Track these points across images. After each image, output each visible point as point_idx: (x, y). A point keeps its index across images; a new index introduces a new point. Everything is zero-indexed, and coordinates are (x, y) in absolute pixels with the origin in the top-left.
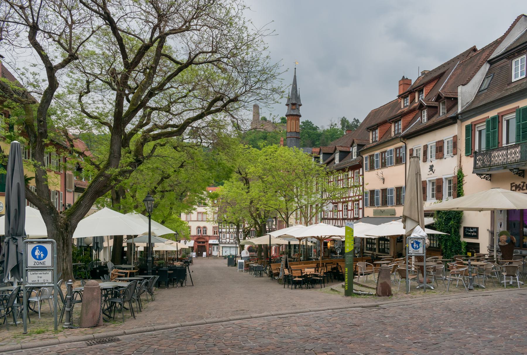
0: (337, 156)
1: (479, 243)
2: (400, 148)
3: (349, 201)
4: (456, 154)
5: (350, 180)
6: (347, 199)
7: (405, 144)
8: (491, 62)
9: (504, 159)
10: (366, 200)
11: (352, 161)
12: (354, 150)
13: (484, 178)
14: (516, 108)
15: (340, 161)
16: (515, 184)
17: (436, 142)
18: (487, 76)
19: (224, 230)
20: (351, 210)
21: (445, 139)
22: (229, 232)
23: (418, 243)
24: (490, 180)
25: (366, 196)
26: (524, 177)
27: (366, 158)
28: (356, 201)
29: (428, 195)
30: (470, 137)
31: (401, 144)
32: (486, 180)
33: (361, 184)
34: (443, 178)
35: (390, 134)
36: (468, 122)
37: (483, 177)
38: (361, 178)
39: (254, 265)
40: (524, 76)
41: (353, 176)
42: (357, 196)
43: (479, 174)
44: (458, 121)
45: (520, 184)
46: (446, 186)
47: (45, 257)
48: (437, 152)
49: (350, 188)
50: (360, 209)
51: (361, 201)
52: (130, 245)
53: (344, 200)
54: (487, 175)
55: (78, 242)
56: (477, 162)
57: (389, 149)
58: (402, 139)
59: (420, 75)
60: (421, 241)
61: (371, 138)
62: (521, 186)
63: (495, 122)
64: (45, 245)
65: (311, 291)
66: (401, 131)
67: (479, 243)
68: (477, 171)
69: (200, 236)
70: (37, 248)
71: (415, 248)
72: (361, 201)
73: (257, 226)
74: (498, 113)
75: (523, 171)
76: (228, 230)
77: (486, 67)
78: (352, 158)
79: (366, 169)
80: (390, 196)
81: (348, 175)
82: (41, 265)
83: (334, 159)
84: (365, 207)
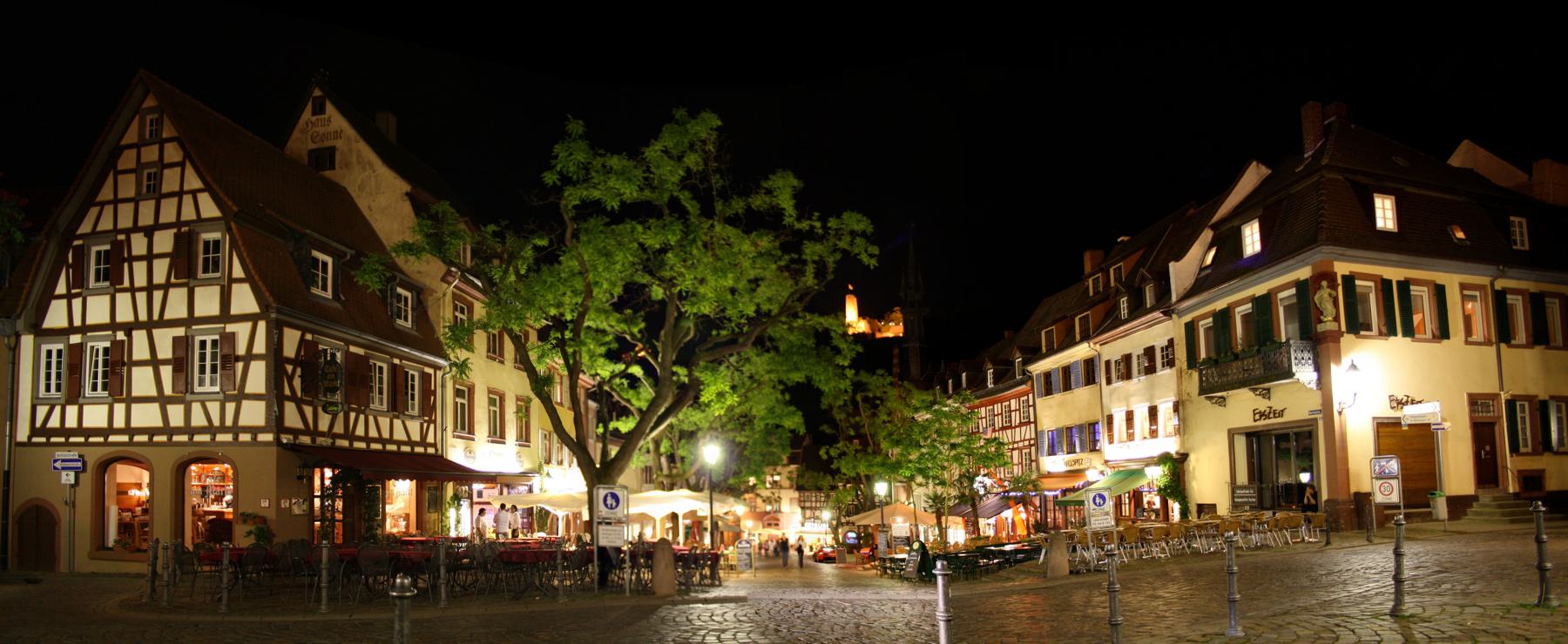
1: (1215, 505)
8: (1213, 227)
13: (1259, 395)
23: (1102, 497)
33: (1032, 420)
34: (1400, 335)
37: (1214, 401)
38: (1031, 409)
39: (1401, 164)
49: (1016, 427)
50: (1032, 461)
55: (686, 519)
60: (1106, 494)
65: (1068, 361)
67: (1215, 505)
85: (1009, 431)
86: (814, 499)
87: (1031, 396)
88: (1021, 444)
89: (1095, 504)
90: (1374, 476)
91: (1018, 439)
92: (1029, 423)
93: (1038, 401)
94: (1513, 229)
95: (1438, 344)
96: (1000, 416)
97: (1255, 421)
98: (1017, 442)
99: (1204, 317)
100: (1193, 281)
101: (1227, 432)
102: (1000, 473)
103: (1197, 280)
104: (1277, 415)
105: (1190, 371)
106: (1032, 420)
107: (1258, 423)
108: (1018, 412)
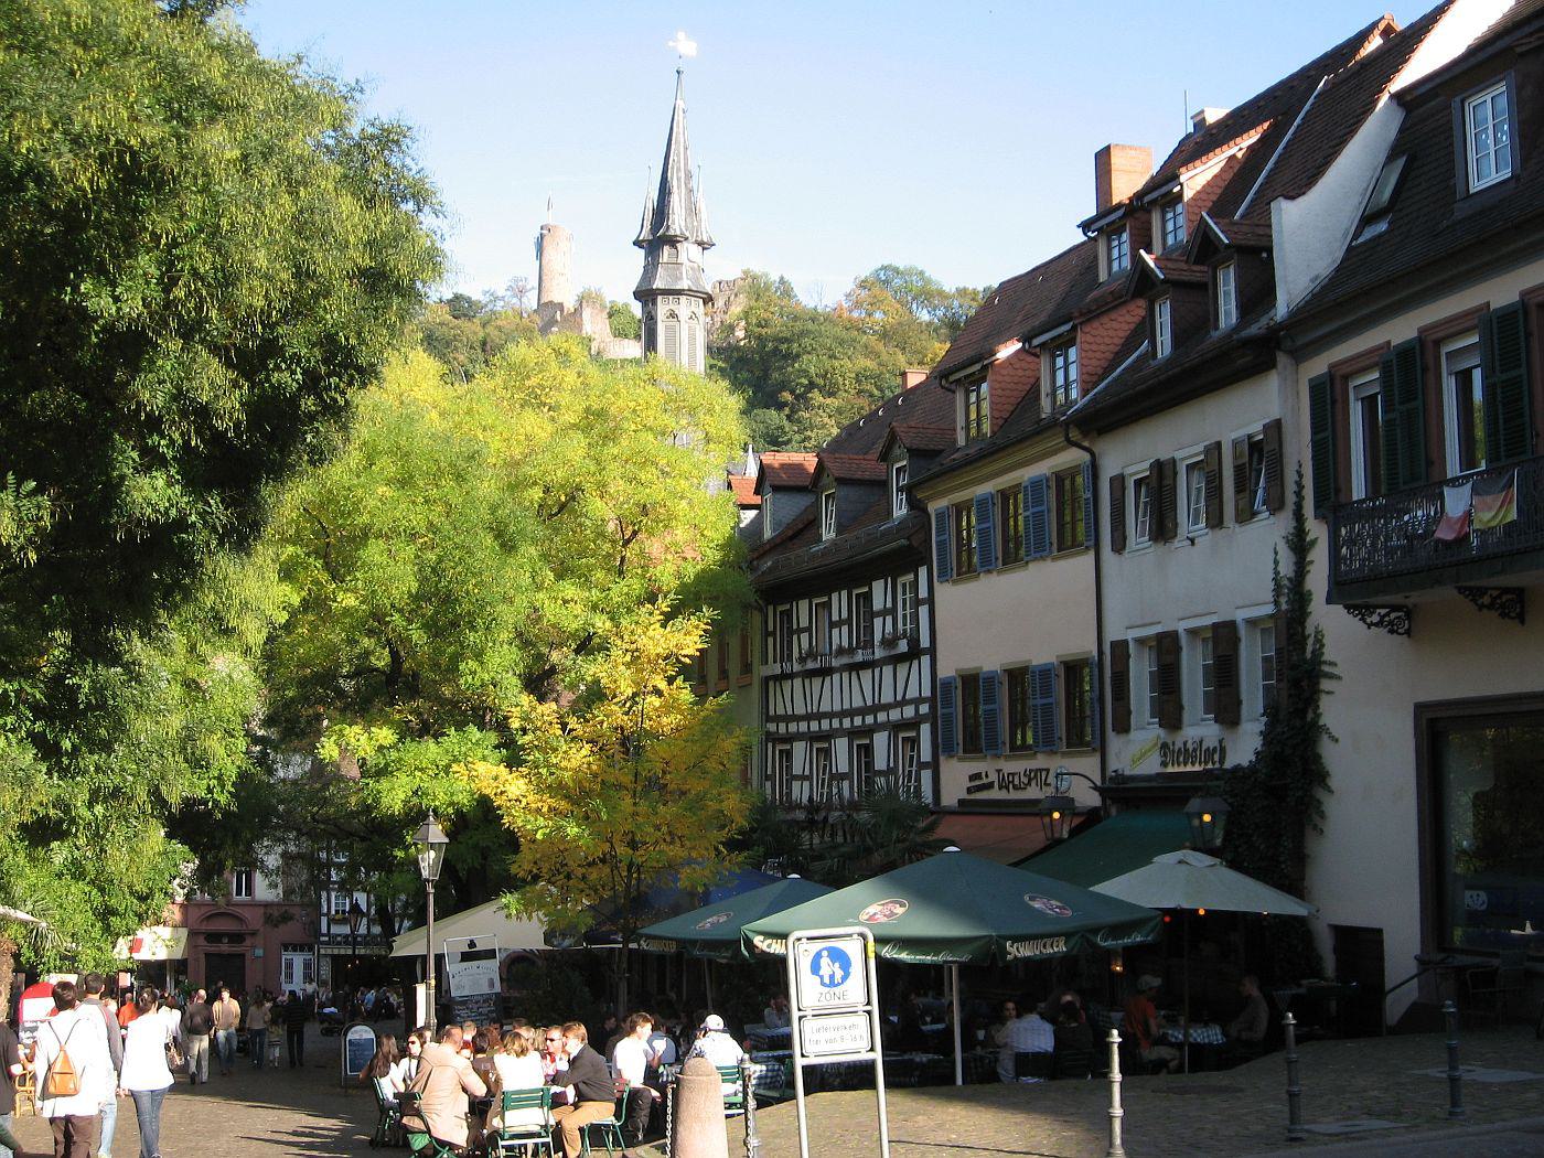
1: (1380, 931)
2: (1072, 472)
3: (877, 727)
6: (869, 720)
7: (1093, 454)
10: (948, 719)
11: (814, 556)
13: (1490, 607)
14: (1478, 309)
21: (1183, 459)
24: (1408, 632)
25: (948, 702)
26: (1522, 622)
27: (940, 515)
29: (1185, 701)
30: (1523, 370)
31: (1071, 457)
32: (1391, 632)
34: (1181, 630)
35: (1039, 409)
36: (1318, 366)
37: (1486, 600)
38: (923, 611)
40: (1506, 173)
41: (889, 605)
43: (1355, 607)
44: (1282, 359)
51: (925, 729)
52: (740, 833)
53: (858, 721)
54: (1394, 608)
57: (1027, 474)
58: (1074, 434)
59: (1191, 129)
61: (960, 422)
66: (1074, 394)
67: (1380, 931)
70: (825, 953)
71: (827, 980)
72: (925, 729)
74: (1422, 331)
75: (1520, 592)
78: (890, 513)
80: (1040, 702)
81: (868, 597)
82: (837, 1002)
87: (923, 571)
88: (895, 715)
91: (887, 698)
93: (944, 592)
94: (1232, 143)
95: (975, 583)
96: (845, 629)
98: (887, 707)
99: (1358, 364)
100: (1340, 255)
101: (1411, 709)
103: (1350, 249)
106: (925, 642)
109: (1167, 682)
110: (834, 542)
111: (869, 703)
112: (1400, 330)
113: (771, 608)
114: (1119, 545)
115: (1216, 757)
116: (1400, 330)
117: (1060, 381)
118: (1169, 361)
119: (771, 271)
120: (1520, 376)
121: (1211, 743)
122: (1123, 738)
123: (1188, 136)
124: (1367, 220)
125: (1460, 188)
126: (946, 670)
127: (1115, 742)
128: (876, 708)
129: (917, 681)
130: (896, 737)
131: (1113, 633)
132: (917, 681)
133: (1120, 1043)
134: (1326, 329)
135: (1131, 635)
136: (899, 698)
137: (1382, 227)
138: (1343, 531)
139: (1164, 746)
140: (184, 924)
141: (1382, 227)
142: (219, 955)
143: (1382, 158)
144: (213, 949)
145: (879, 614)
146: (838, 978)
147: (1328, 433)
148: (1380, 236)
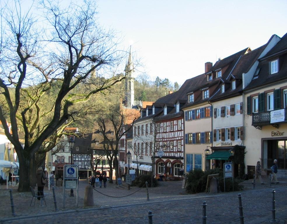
0: (166, 110)
3: (174, 140)
4: (242, 113)
5: (175, 126)
6: (173, 139)
7: (211, 104)
9: (268, 118)
12: (178, 107)
13: (257, 128)
15: (168, 113)
16: (273, 132)
17: (231, 106)
18: (258, 68)
19: (77, 159)
20: (176, 146)
22: (88, 160)
24: (261, 129)
27: (186, 112)
28: (179, 140)
30: (280, 97)
31: (209, 105)
33: (183, 129)
36: (248, 95)
41: (177, 124)
42: (180, 137)
44: (243, 94)
45: (276, 132)
46: (218, 134)
47: (73, 173)
48: (221, 113)
49: (168, 132)
51: (182, 141)
53: (171, 139)
56: (254, 119)
58: (210, 102)
62: (276, 133)
63: (250, 99)
64: (229, 165)
68: (255, 124)
69: (59, 163)
71: (70, 173)
72: (182, 141)
73: (114, 157)
76: (80, 159)
77: (256, 64)
79: (186, 120)
83: (163, 112)
84: (185, 145)
85: (172, 133)
86: (80, 157)
88: (177, 139)
89: (69, 173)
90: (183, 132)
92: (181, 130)
96: (169, 127)
97: (272, 136)
99: (255, 95)
100: (251, 81)
102: (168, 149)
103: (252, 80)
104: (280, 134)
105: (248, 115)
107: (273, 137)
108: (177, 126)
109: (223, 134)
110: (166, 116)
111: (173, 137)
112: (261, 91)
113: (156, 124)
114: (216, 117)
115: (230, 145)
116: (261, 91)
117: (191, 99)
118: (224, 94)
119: (208, 61)
120: (279, 98)
121: (230, 143)
122: (215, 142)
123: (218, 61)
124: (254, 76)
125: (270, 73)
126: (186, 133)
127: (214, 142)
128: (174, 138)
129: (181, 134)
130: (177, 142)
131: (214, 128)
132: (181, 134)
133: (12, 175)
134: (249, 91)
135: (217, 129)
136: (178, 136)
137: (257, 77)
138: (254, 117)
139: (222, 143)
140: (105, 165)
141: (257, 77)
142: (59, 170)
143: (256, 68)
144: (59, 169)
145: (175, 125)
146: (72, 172)
147: (250, 104)
148: (256, 79)
